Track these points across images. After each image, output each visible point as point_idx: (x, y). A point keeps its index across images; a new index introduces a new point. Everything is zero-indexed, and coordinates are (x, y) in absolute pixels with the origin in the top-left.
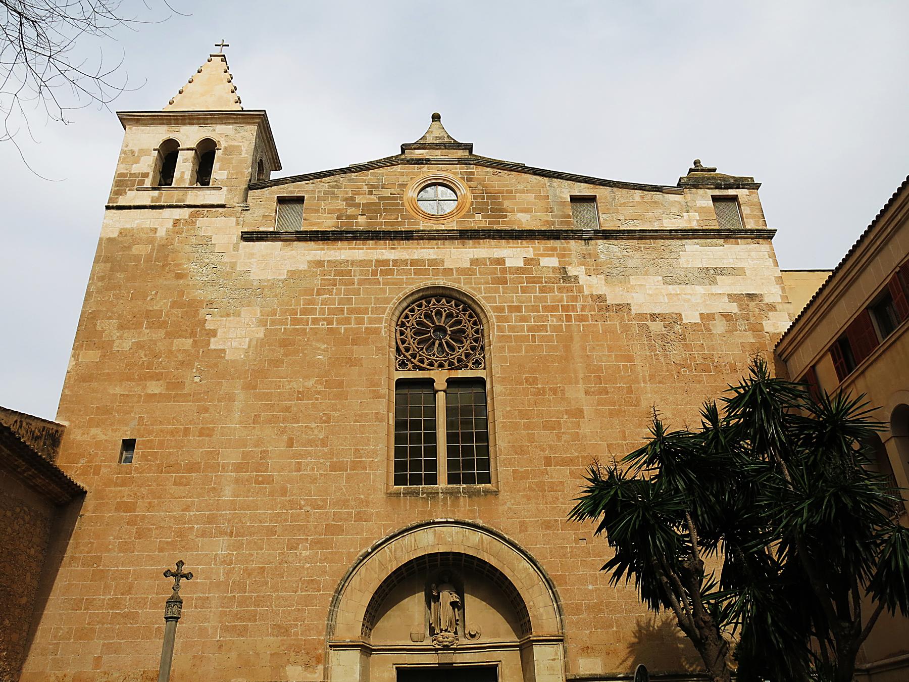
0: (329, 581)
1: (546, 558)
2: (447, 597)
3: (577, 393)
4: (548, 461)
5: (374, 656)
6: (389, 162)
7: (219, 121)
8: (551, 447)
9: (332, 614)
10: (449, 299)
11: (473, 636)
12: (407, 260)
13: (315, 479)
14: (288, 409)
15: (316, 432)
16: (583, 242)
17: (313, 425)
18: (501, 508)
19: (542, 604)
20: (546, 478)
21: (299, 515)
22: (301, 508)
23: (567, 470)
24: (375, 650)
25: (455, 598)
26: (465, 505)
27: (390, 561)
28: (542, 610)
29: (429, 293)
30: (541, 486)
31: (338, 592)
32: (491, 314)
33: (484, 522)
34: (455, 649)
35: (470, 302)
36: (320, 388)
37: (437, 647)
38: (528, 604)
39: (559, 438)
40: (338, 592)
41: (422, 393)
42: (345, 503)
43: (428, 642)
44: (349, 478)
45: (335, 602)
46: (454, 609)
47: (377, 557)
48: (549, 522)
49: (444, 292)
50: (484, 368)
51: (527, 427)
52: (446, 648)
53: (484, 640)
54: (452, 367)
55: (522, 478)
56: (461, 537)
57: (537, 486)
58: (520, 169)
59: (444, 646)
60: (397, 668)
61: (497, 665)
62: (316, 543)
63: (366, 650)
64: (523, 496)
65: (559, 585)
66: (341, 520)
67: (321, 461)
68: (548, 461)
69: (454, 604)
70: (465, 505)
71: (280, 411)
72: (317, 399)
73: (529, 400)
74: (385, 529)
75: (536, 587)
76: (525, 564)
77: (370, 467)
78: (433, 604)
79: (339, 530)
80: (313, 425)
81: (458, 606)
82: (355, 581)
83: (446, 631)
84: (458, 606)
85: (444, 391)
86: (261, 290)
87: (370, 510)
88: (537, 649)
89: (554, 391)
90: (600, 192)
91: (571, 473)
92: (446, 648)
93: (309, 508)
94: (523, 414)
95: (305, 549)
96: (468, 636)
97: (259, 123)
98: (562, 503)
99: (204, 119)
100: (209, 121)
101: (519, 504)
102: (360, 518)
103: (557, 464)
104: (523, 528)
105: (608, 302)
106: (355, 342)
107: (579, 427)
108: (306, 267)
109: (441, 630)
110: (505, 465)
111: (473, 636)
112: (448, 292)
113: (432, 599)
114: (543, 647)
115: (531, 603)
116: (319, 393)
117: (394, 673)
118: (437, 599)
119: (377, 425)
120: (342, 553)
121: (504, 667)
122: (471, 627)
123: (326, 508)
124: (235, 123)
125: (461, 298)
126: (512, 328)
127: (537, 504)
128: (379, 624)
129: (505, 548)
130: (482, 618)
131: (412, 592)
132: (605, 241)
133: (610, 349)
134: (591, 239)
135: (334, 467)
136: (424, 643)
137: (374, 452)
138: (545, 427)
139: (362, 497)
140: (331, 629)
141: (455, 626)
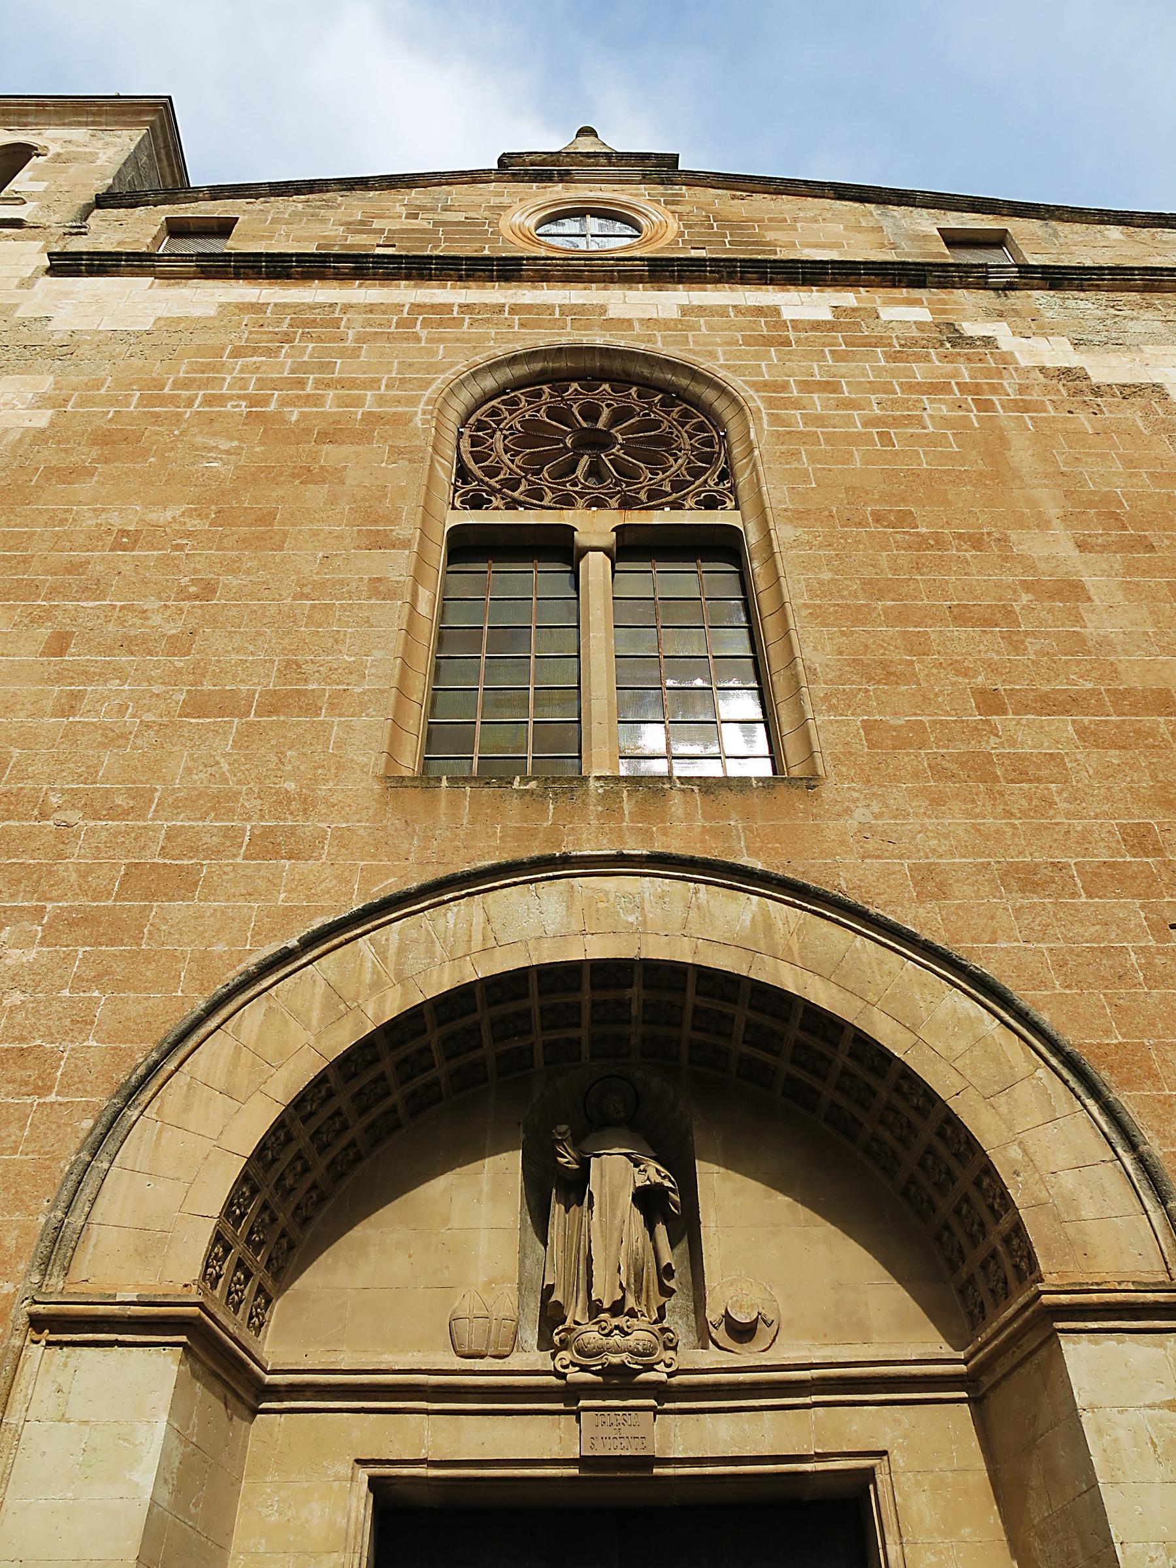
0: (96, 1057)
1: (1044, 984)
2: (617, 1174)
3: (1053, 547)
4: (990, 702)
5: (272, 1429)
6: (473, 177)
7: (55, 119)
8: (991, 667)
9: (80, 1184)
10: (621, 381)
11: (742, 1332)
12: (503, 306)
13: (122, 736)
14: (74, 568)
15: (156, 620)
16: (992, 292)
17: (152, 604)
18: (832, 828)
19: (1062, 1158)
20: (991, 745)
21: (29, 835)
22: (44, 816)
23: (1065, 726)
24: (276, 1392)
25: (653, 1173)
26: (689, 816)
27: (377, 985)
28: (1068, 1180)
29: (562, 364)
30: (981, 768)
31: (131, 1093)
32: (755, 400)
33: (841, 254)
34: (661, 1392)
35: (684, 382)
36: (195, 524)
37: (575, 1376)
38: (1004, 1157)
39: (1017, 646)
40: (131, 1093)
41: (539, 579)
42: (221, 803)
43: (529, 1358)
44: (247, 734)
45: (109, 1130)
46: (650, 1226)
47: (324, 969)
48: (1034, 869)
49: (607, 363)
50: (737, 508)
51: (900, 617)
52: (619, 1382)
53: (793, 1350)
54: (627, 504)
55: (902, 743)
56: (678, 911)
57: (962, 765)
58: (804, 189)
59: (609, 1371)
60: (374, 1483)
61: (868, 1475)
62: (72, 924)
63: (231, 1379)
64: (913, 794)
65: (1128, 1083)
66: (193, 851)
67: (157, 689)
68: (990, 702)
69: (648, 1201)
70: (689, 816)
71: (46, 573)
72: (180, 547)
73: (893, 559)
74: (365, 881)
75: (1023, 1091)
76: (959, 1003)
77: (332, 707)
78: (557, 1209)
79: (184, 883)
80: (152, 604)
81: (670, 1211)
82: (212, 1056)
83: (617, 1309)
84: (670, 1211)
85: (607, 551)
86: (66, 350)
87: (311, 825)
88: (1084, 1357)
89: (977, 543)
90: (1013, 225)
91: (1083, 733)
92: (619, 1382)
93: (74, 816)
94: (875, 588)
95: (24, 942)
96: (720, 1334)
97: (152, 124)
98: (1068, 815)
99: (14, 113)
100: (30, 119)
101: (900, 813)
102: (267, 845)
103: (1023, 708)
104: (930, 886)
105: (1094, 380)
106: (326, 437)
107: (1078, 619)
108: (212, 313)
109: (594, 1309)
110: (832, 708)
111: (742, 1332)
112: (617, 365)
113: (554, 1188)
114: (1110, 1343)
115: (1015, 1152)
116: (190, 535)
117: (357, 1508)
118: (575, 1188)
119: (371, 607)
120: (173, 957)
121: (905, 1481)
122: (727, 1293)
123: (142, 816)
124: (94, 123)
125: (658, 374)
126: (819, 420)
127: (969, 814)
128: (310, 1280)
129: (866, 950)
130: (782, 1263)
131: (466, 1150)
132: (1052, 293)
133: (1129, 462)
134: (1010, 287)
135: (197, 705)
136: (512, 1363)
137: (356, 671)
138: (960, 616)
139: (291, 786)
140: (57, 1248)
141: (657, 1300)
